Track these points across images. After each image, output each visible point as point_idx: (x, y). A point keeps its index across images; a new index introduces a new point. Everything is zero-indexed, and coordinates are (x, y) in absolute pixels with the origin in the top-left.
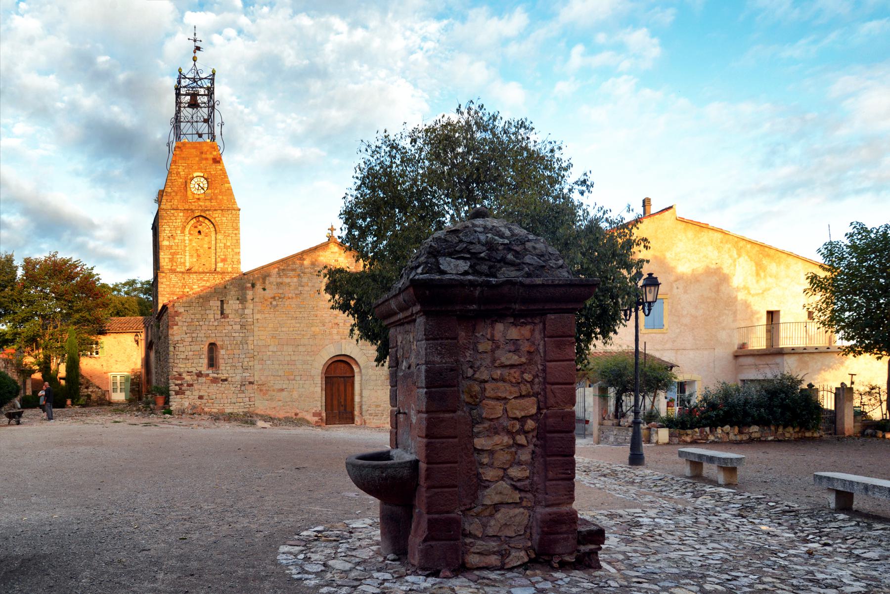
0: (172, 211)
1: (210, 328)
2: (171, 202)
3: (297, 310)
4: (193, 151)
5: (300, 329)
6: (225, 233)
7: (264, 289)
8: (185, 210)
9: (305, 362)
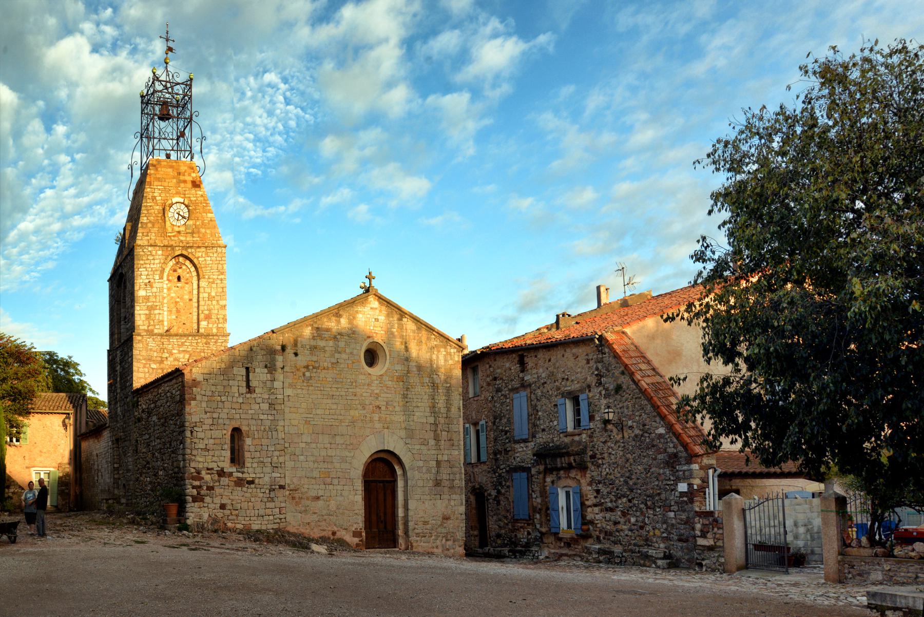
0: (150, 249)
2: (147, 236)
3: (334, 386)
4: (170, 170)
5: (338, 412)
6: (209, 278)
7: (296, 354)
8: (164, 246)
9: (343, 460)
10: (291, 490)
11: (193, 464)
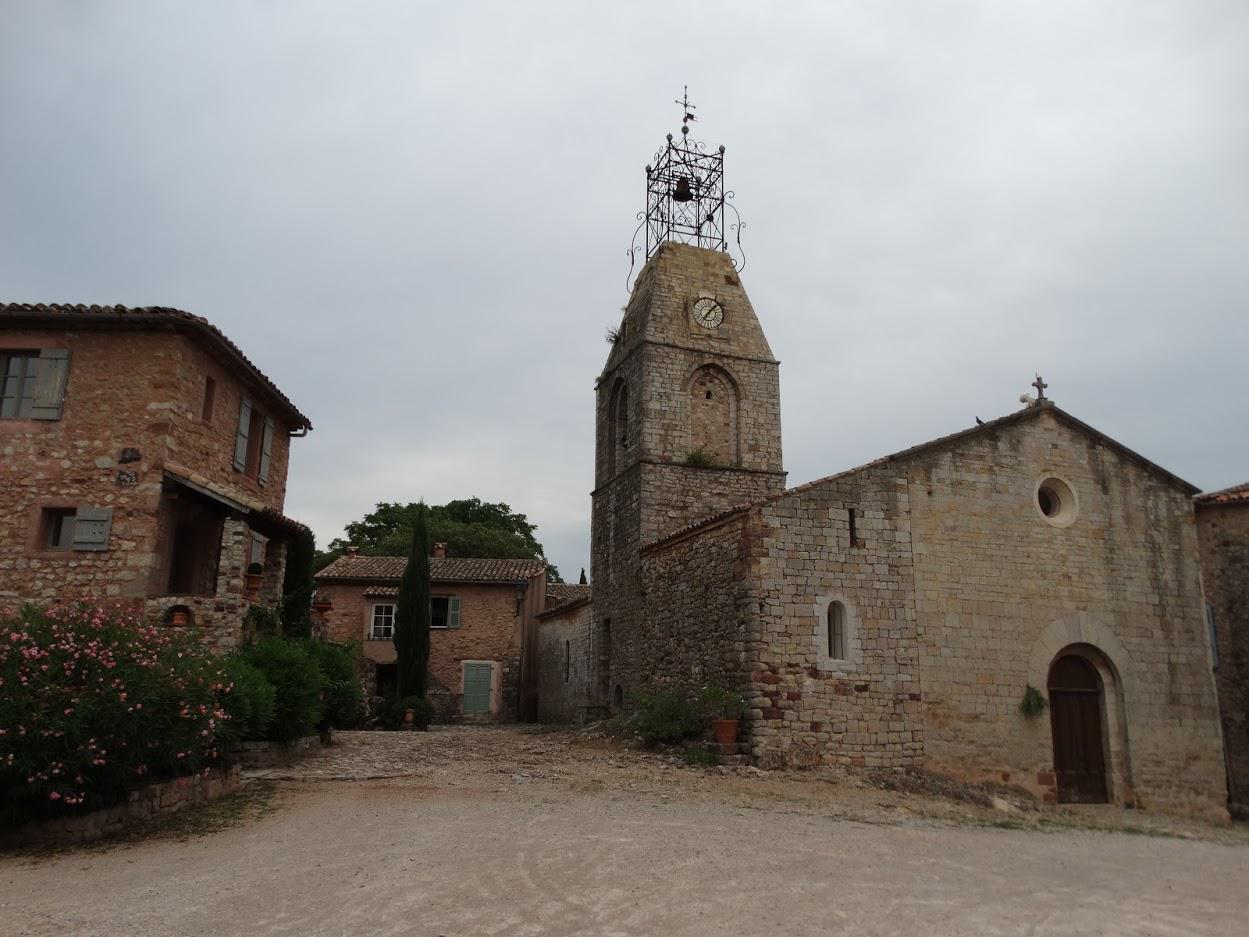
0: (667, 349)
1: (832, 567)
2: (662, 332)
8: (688, 349)
10: (930, 703)
11: (765, 657)
